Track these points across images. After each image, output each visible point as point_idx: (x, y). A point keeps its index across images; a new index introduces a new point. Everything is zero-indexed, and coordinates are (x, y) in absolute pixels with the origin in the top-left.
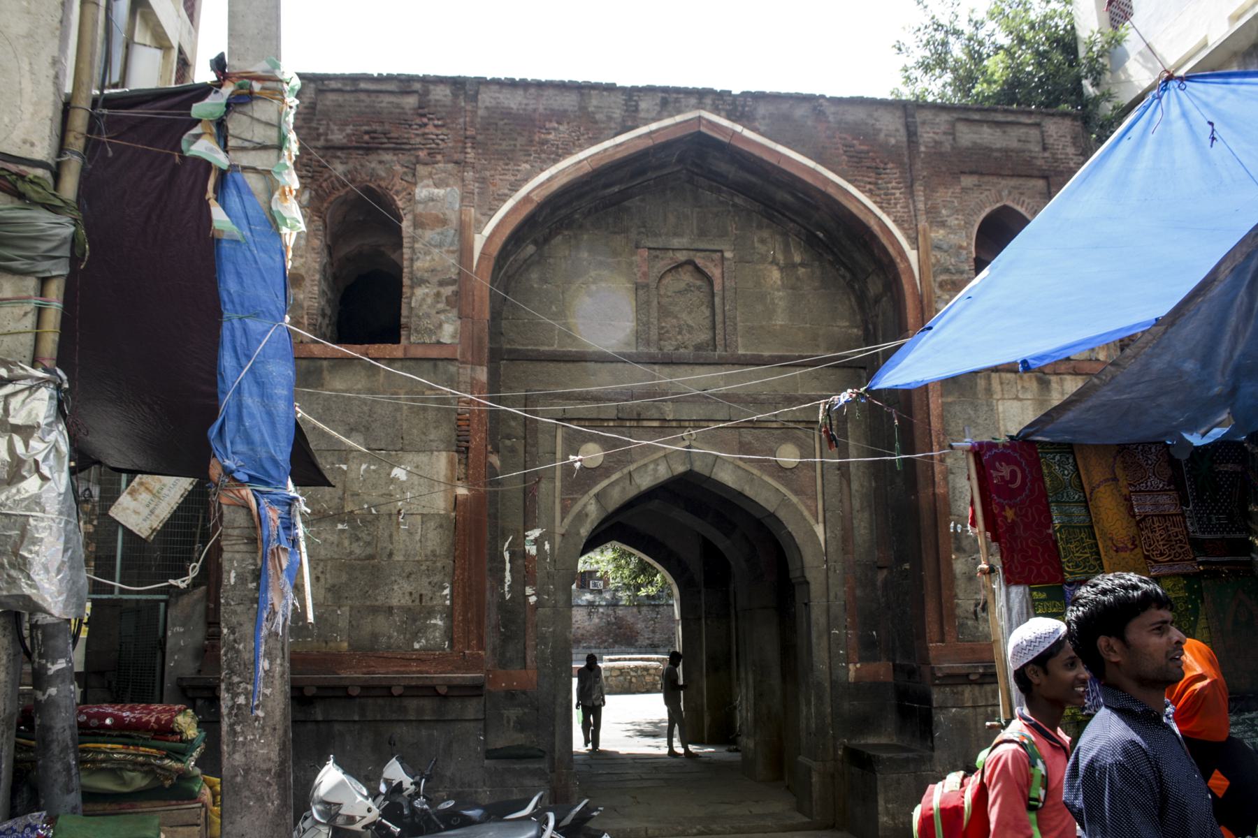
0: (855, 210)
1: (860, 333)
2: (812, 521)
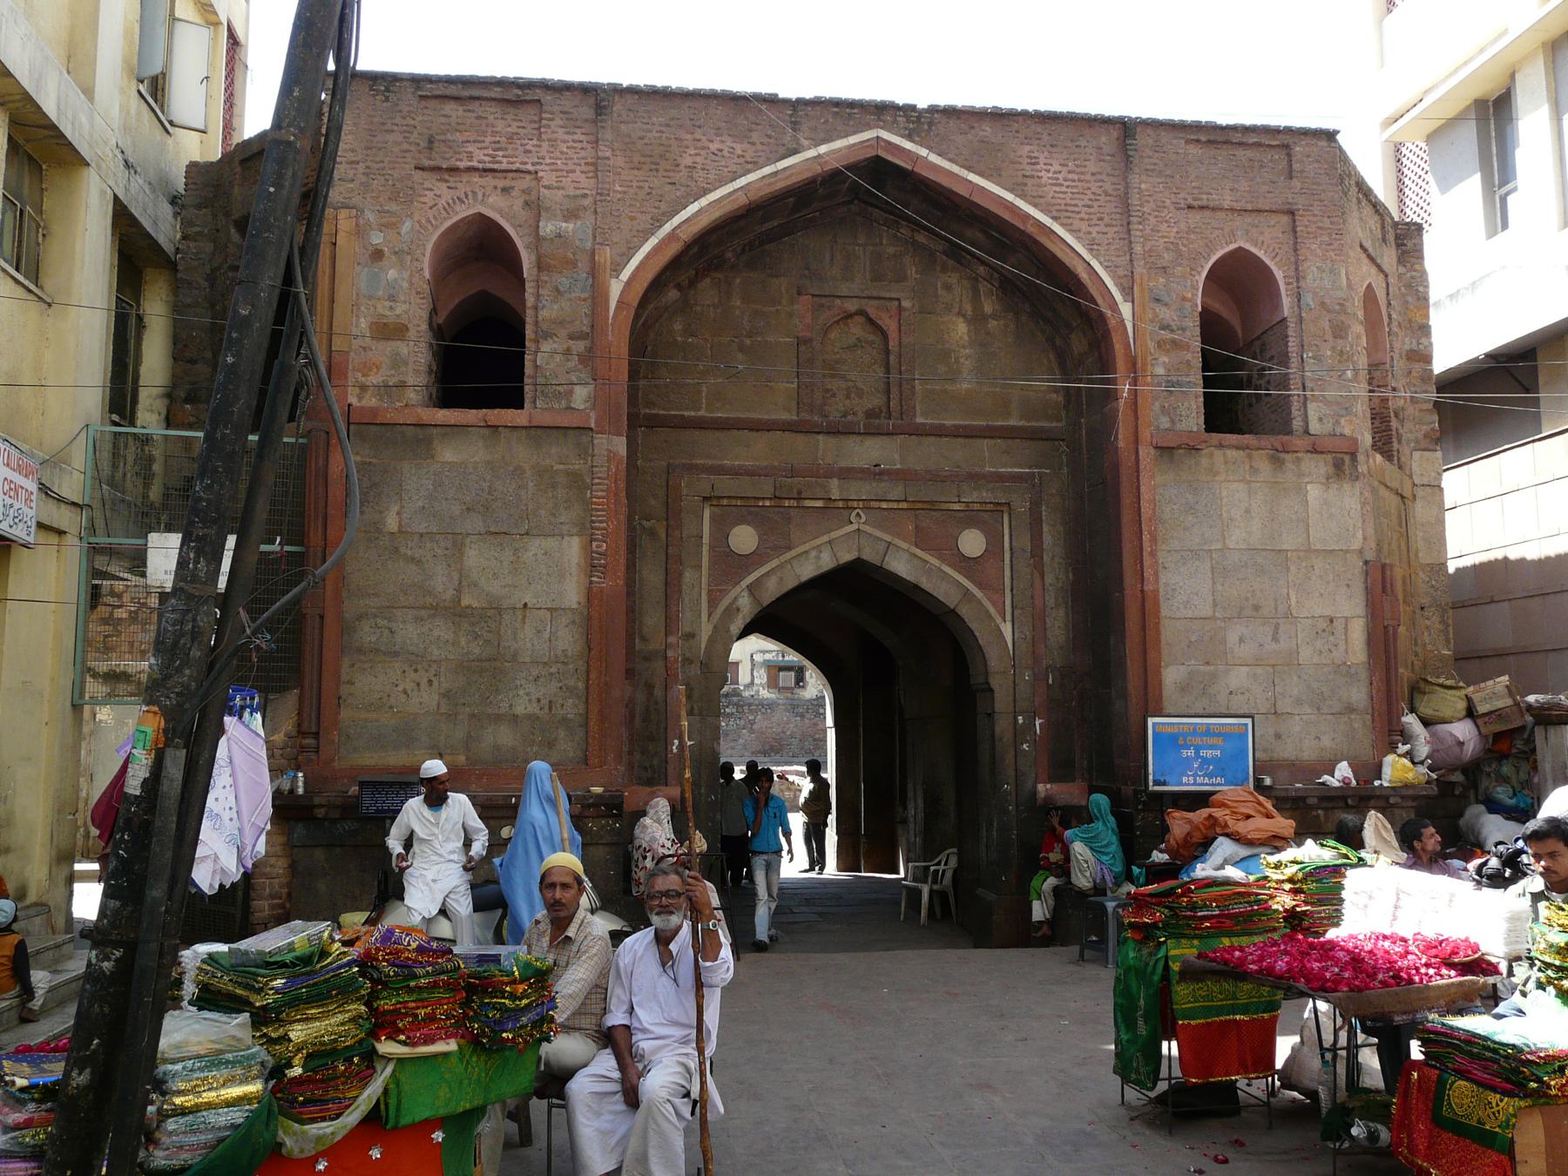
2: (999, 620)
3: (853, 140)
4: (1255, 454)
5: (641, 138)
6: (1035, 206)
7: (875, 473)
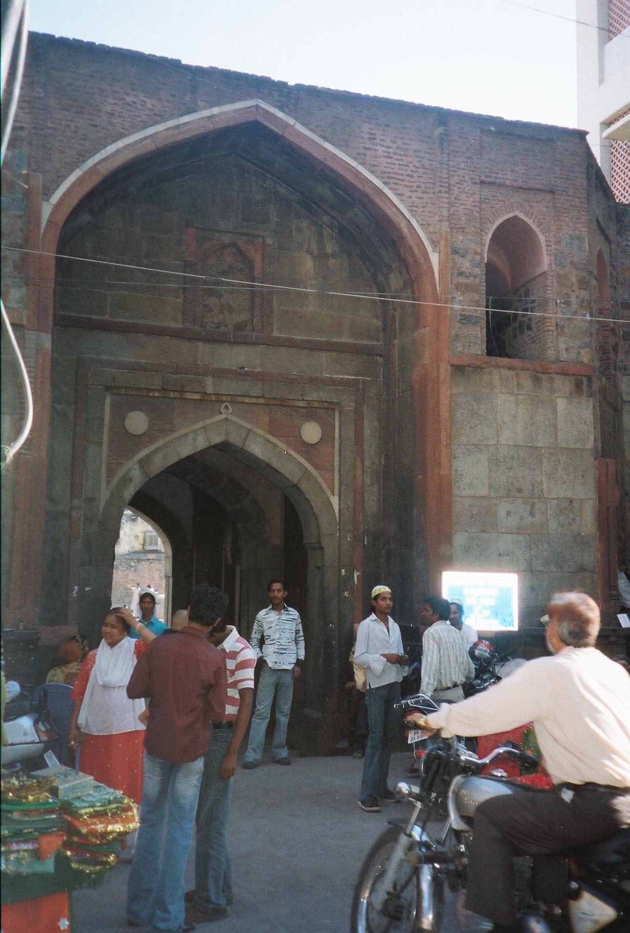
0: (389, 212)
1: (380, 323)
2: (329, 493)
3: (239, 105)
4: (522, 373)
5: (70, 85)
6: (372, 172)
7: (241, 374)
